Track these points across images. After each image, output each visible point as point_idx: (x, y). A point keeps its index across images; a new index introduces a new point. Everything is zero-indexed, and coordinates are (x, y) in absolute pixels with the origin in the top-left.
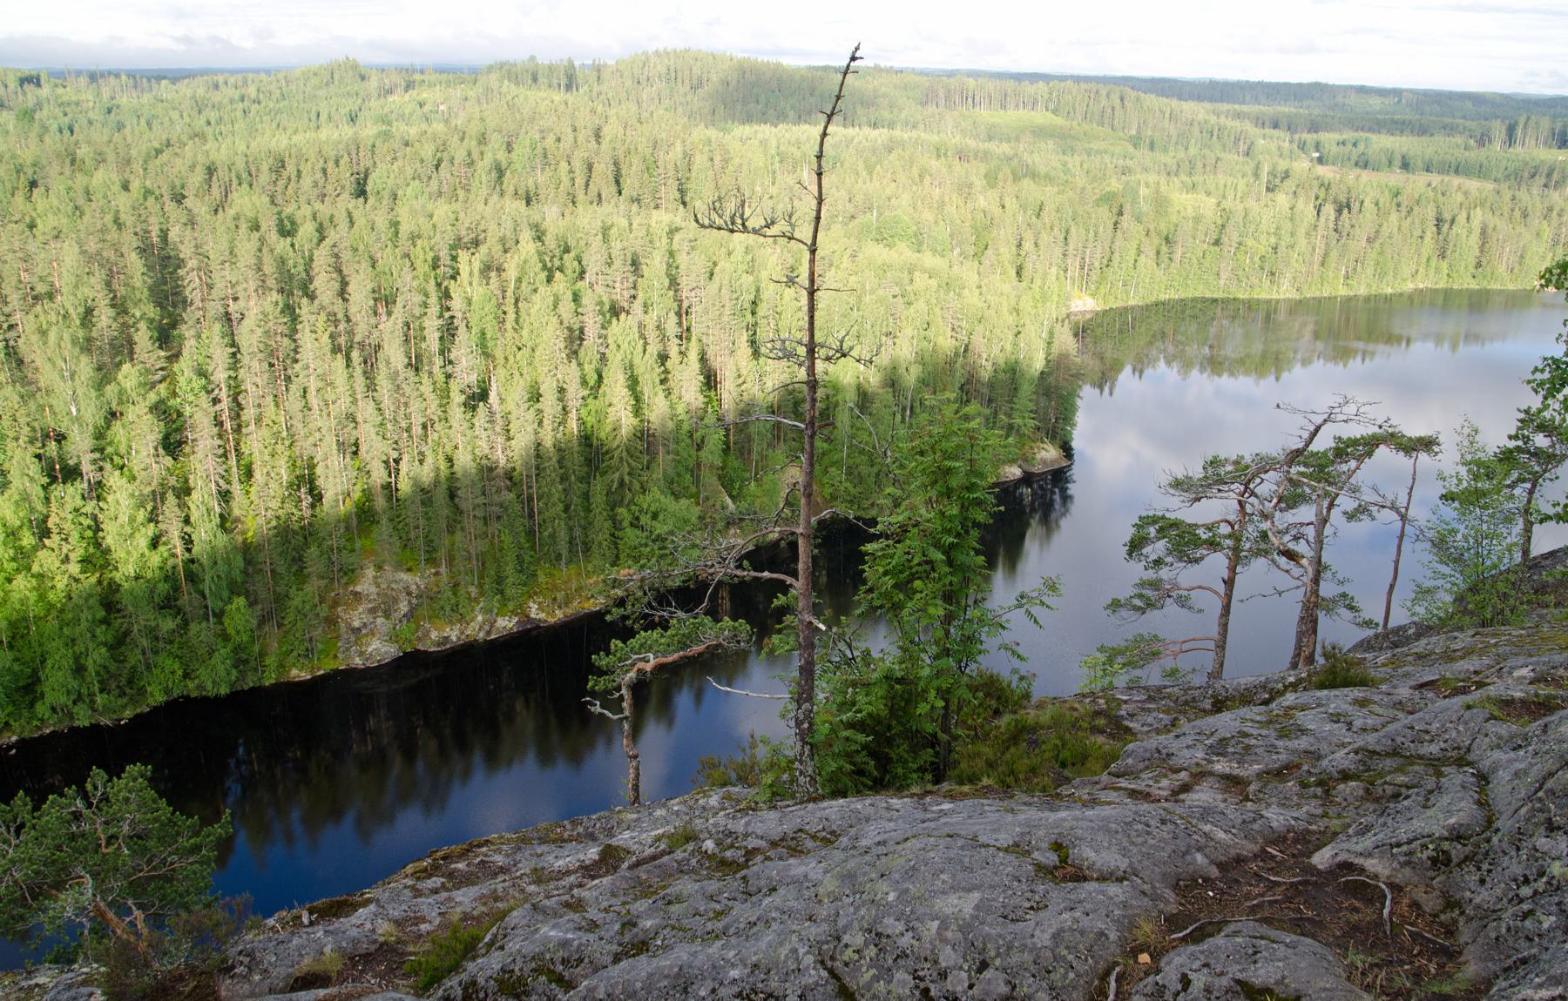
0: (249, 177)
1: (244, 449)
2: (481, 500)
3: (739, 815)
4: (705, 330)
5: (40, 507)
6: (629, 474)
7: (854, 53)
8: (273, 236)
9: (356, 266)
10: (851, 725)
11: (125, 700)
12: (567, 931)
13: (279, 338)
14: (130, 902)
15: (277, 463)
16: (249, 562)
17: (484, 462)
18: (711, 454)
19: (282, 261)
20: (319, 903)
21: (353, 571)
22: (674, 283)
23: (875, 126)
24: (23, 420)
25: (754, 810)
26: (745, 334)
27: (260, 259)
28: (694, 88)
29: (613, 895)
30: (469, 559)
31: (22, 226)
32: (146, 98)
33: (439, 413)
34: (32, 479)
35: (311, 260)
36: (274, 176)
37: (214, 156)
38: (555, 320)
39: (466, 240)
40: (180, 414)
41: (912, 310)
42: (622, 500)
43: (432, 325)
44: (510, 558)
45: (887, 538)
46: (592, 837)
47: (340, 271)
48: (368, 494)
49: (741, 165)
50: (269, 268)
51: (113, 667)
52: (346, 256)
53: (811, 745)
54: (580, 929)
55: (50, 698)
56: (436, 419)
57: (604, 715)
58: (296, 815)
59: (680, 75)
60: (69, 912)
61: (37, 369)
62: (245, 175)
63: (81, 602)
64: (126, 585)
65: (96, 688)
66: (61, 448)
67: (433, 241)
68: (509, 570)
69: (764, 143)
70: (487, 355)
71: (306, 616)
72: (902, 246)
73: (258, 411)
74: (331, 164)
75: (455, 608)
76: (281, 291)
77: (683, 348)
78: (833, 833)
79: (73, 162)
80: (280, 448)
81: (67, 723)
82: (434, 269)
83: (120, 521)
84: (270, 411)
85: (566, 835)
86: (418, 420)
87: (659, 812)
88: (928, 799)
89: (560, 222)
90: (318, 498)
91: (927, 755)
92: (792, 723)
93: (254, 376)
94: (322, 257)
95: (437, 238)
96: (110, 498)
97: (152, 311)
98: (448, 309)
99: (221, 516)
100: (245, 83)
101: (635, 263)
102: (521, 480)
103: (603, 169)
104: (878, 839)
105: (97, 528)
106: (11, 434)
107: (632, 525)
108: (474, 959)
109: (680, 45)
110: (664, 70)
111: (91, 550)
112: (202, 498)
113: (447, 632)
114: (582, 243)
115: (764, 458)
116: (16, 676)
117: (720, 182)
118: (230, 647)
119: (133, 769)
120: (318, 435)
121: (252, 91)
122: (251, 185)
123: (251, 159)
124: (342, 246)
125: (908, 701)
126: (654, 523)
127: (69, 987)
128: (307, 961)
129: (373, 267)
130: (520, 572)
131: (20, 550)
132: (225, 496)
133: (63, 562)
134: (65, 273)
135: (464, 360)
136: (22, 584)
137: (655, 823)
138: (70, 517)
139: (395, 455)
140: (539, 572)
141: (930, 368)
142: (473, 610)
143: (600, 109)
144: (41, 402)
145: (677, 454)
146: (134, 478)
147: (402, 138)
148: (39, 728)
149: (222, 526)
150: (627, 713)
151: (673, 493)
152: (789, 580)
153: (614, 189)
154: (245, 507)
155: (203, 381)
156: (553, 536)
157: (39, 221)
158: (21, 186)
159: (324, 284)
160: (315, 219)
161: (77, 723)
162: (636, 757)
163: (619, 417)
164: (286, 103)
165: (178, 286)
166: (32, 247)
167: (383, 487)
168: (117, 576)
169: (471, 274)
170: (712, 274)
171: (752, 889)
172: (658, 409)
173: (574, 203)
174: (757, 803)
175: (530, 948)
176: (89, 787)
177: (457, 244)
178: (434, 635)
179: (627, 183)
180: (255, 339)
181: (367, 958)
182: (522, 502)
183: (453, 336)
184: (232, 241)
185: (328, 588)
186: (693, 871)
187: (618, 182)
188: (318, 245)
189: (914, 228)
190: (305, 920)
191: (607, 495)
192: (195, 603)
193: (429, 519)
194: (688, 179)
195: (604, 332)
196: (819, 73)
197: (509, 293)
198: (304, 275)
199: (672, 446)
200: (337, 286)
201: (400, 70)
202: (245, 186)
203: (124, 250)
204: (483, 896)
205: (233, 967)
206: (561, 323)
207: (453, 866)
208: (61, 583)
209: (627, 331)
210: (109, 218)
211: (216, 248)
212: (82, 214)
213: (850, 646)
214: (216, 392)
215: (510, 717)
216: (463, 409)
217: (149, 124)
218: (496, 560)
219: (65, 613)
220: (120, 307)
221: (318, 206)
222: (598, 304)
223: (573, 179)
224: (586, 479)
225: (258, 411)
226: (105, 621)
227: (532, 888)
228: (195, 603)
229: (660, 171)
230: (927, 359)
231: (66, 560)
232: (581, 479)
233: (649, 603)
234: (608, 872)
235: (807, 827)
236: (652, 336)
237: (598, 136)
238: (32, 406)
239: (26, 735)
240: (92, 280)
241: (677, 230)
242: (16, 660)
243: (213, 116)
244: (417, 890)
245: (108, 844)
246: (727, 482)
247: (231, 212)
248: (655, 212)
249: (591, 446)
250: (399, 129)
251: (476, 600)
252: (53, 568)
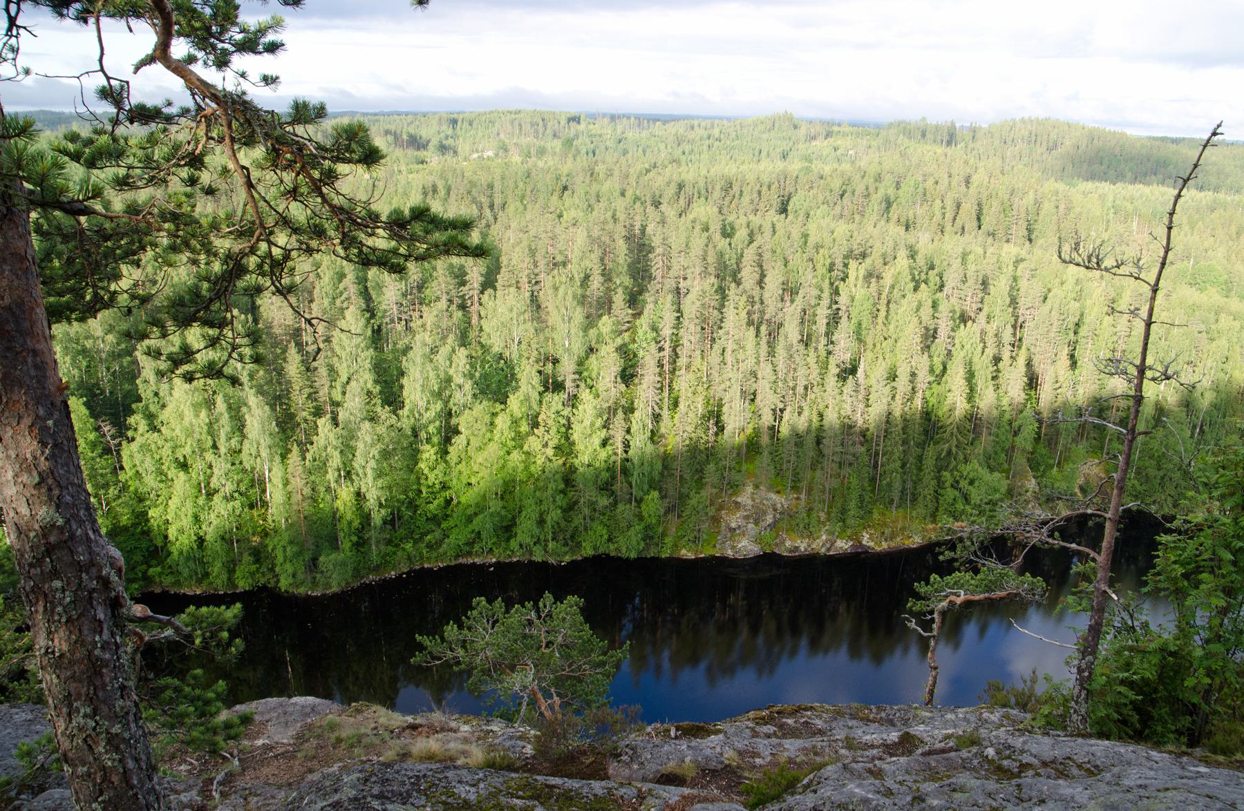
0: (706, 193)
1: (675, 386)
2: (839, 449)
3: (1017, 733)
4: (1033, 342)
5: (535, 407)
6: (956, 446)
7: (1216, 129)
8: (717, 236)
9: (773, 264)
10: (1123, 682)
11: (567, 549)
12: (868, 792)
13: (711, 310)
14: (553, 690)
15: (696, 400)
16: (665, 467)
17: (846, 420)
18: (1025, 440)
19: (721, 255)
20: (685, 724)
21: (737, 486)
22: (1014, 302)
23: (1201, 189)
24: (534, 346)
25: (1030, 732)
26: (1066, 349)
27: (706, 252)
28: (1049, 150)
29: (907, 772)
30: (824, 492)
31: (554, 216)
32: (645, 134)
33: (818, 379)
34: (533, 387)
35: (742, 256)
36: (723, 194)
37: (684, 176)
38: (916, 320)
39: (856, 252)
40: (635, 355)
41: (1214, 344)
42: (947, 466)
43: (823, 313)
44: (854, 496)
45: (1180, 534)
46: (892, 723)
47: (761, 266)
48: (757, 432)
49: (1081, 213)
50: (711, 259)
51: (563, 524)
52: (767, 256)
53: (1088, 690)
54: (878, 793)
55: (520, 538)
56: (815, 383)
57: (916, 630)
58: (666, 654)
59: (1039, 139)
60: (517, 688)
61: (548, 313)
62: (703, 192)
63: (550, 476)
64: (581, 470)
65: (550, 537)
66: (554, 368)
67: (831, 251)
68: (852, 504)
69: (1102, 197)
70: (860, 340)
71: (698, 513)
72: (1212, 291)
73: (689, 360)
74: (765, 188)
75: (807, 526)
76: (717, 276)
77: (1014, 354)
78: (1096, 767)
79: (592, 175)
80: (700, 389)
81: (527, 557)
82: (830, 272)
83: (584, 424)
84: (697, 362)
85: (871, 716)
86: (802, 382)
87: (949, 716)
88: (1185, 759)
89: (930, 246)
90: (721, 429)
91: (1186, 721)
92: (1075, 670)
93: (690, 334)
94: (750, 255)
95: (835, 249)
96: (580, 407)
97: (628, 281)
98: (836, 303)
99: (652, 431)
100: (712, 126)
101: (985, 284)
102: (872, 438)
103: (969, 208)
104: (1139, 782)
105: (569, 427)
106: (526, 355)
107: (952, 486)
108: (793, 794)
109: (1040, 114)
110: (1027, 133)
111: (563, 441)
112: (641, 416)
113: (798, 543)
114: (945, 263)
115: (1067, 449)
116: (502, 518)
117: (1062, 226)
118: (643, 524)
119: (572, 599)
120: (728, 383)
121: (716, 132)
122: (707, 199)
123: (709, 180)
124: (765, 248)
125: (1176, 672)
126: (970, 487)
127: (511, 738)
128: (672, 764)
129: (785, 266)
130: (860, 508)
131: (518, 433)
132: (657, 418)
133: (543, 446)
134: (576, 249)
135: (842, 342)
136: (516, 456)
137: (946, 724)
138: (553, 416)
139: (781, 406)
140: (874, 511)
141: (1224, 396)
142: (820, 531)
143: (972, 161)
144: (547, 335)
145: (997, 436)
146: (598, 396)
147: (819, 173)
148: (510, 556)
149: (651, 439)
150: (935, 633)
151: (989, 467)
152: (1092, 554)
153: (975, 224)
154: (669, 427)
155: (655, 334)
156: (889, 485)
157: (565, 213)
158: (558, 189)
159: (748, 275)
160: (748, 226)
161: (534, 558)
162: (935, 668)
163: (955, 401)
164: (739, 142)
165: (647, 265)
166: (558, 230)
167: (770, 428)
168: (576, 462)
169: (857, 278)
170: (1046, 298)
171: (1025, 797)
172: (987, 400)
173: (942, 232)
174: (1033, 727)
175: (838, 797)
176: (541, 604)
177: (849, 255)
178: (788, 544)
179: (986, 220)
180: (694, 308)
181: (714, 773)
182: (871, 456)
183: (837, 323)
184: (688, 238)
185: (717, 496)
186: (974, 769)
187: (979, 219)
188: (748, 246)
189: (1226, 277)
190: (673, 734)
191: (936, 460)
192: (625, 490)
193: (798, 457)
194: (1036, 221)
195: (952, 334)
196: (1157, 143)
197: (884, 296)
198: (735, 266)
199: (994, 430)
200: (757, 277)
201: (823, 122)
202: (703, 199)
203: (616, 237)
204: (805, 749)
205: (620, 755)
206: (921, 323)
207: (784, 720)
208: (540, 461)
209: (971, 335)
210: (609, 214)
211: (676, 242)
212: (593, 210)
213: (1132, 617)
214: (662, 343)
215: (834, 615)
216: (836, 379)
217: (644, 152)
218: (844, 496)
219: (539, 482)
220: (607, 276)
221: (752, 217)
222: (951, 312)
223: (944, 214)
224: (922, 446)
225: (689, 360)
226: (562, 492)
227: (843, 751)
228: (625, 490)
229: (1014, 213)
230: (1222, 387)
231: (546, 445)
232: (918, 445)
233: (975, 551)
234: (903, 754)
235: (1075, 757)
236: (991, 341)
237: (967, 182)
238: (542, 337)
239: (502, 559)
240: (593, 256)
241: (1022, 260)
242: (504, 507)
243: (687, 148)
244: (755, 732)
245: (547, 646)
246: (1034, 464)
247: (691, 217)
248: (1006, 245)
249: (930, 420)
250: (817, 166)
251: (824, 523)
252: (537, 450)
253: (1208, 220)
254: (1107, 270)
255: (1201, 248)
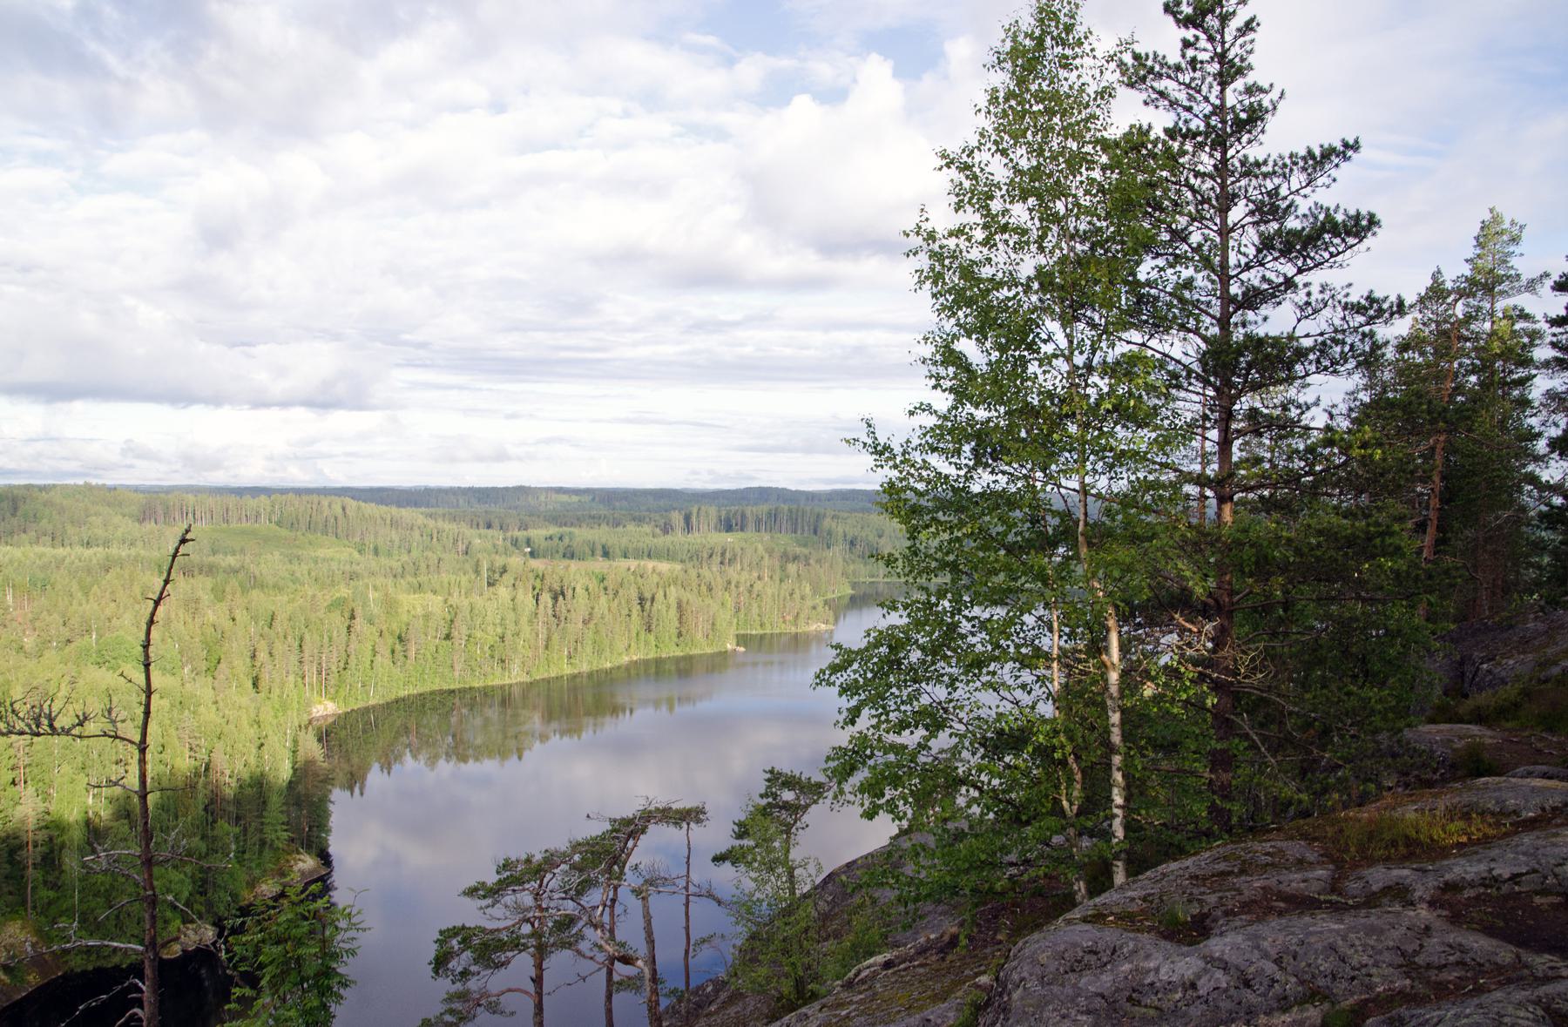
253: (104, 582)
254: (67, 732)
255: (103, 617)
